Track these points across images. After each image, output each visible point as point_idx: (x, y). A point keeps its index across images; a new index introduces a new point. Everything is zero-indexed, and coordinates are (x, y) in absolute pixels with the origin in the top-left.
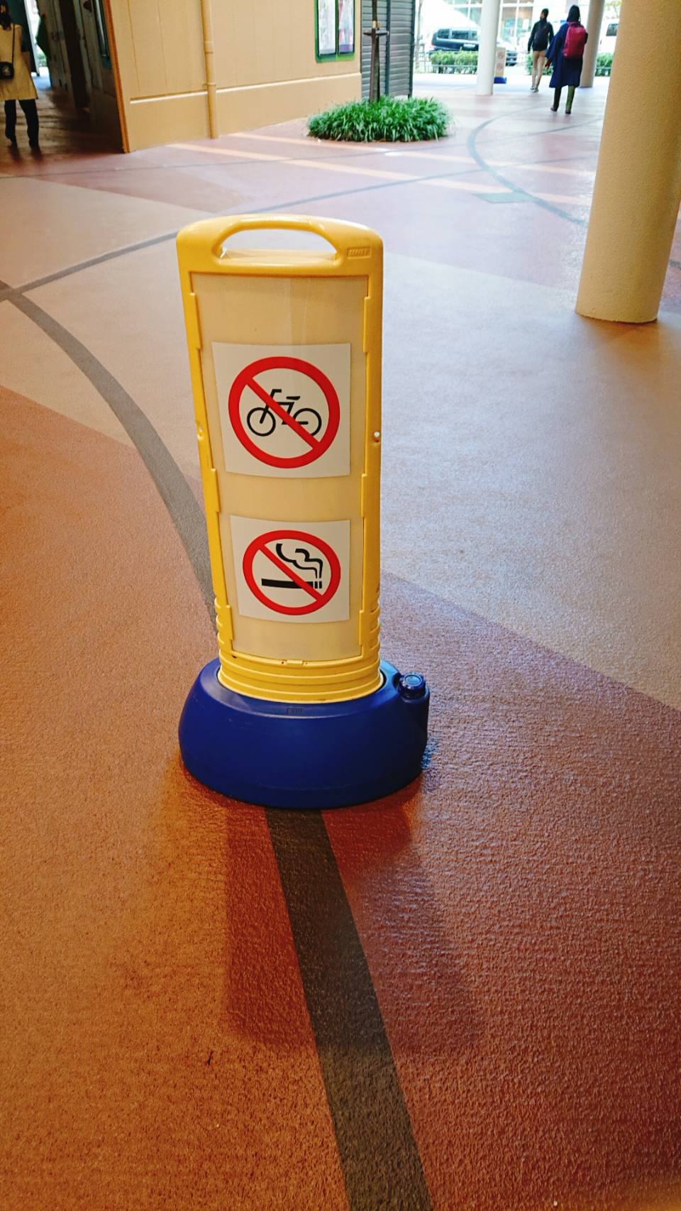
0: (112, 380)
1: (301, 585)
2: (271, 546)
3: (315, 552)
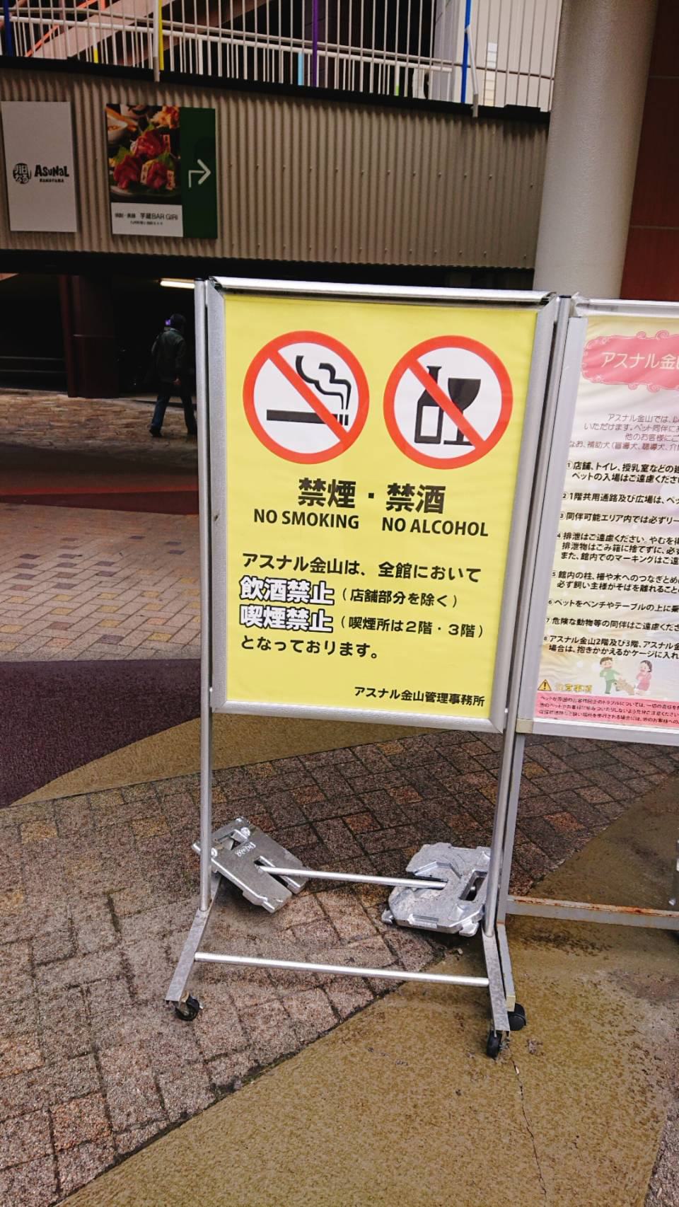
2: (289, 354)
3: (343, 371)
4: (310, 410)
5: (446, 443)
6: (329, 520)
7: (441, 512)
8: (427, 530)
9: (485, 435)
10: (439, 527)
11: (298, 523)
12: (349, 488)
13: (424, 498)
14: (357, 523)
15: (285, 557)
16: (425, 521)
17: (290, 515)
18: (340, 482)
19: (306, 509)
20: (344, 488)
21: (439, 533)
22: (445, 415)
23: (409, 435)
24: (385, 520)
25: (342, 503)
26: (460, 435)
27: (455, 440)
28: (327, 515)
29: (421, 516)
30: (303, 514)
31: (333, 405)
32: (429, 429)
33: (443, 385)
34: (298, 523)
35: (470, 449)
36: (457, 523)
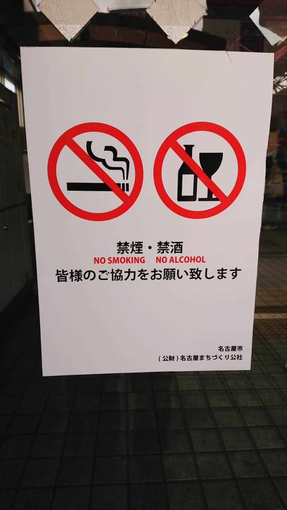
0: (265, 228)
1: (110, 186)
2: (81, 140)
3: (123, 152)
4: (100, 181)
5: (200, 200)
6: (130, 260)
7: (181, 252)
8: (177, 261)
9: (227, 192)
10: (182, 260)
11: (116, 263)
12: (140, 245)
13: (173, 248)
14: (144, 260)
15: (129, 270)
16: (176, 258)
17: (112, 259)
18: (136, 242)
19: (120, 256)
20: (138, 245)
21: (183, 262)
22: (199, 180)
23: (173, 196)
24: (157, 258)
25: (138, 252)
26: (210, 193)
27: (206, 197)
28: (130, 258)
29: (174, 255)
30: (118, 258)
31: (116, 177)
32: (187, 191)
33: (196, 157)
34: (116, 263)
35: (218, 203)
36: (191, 257)
